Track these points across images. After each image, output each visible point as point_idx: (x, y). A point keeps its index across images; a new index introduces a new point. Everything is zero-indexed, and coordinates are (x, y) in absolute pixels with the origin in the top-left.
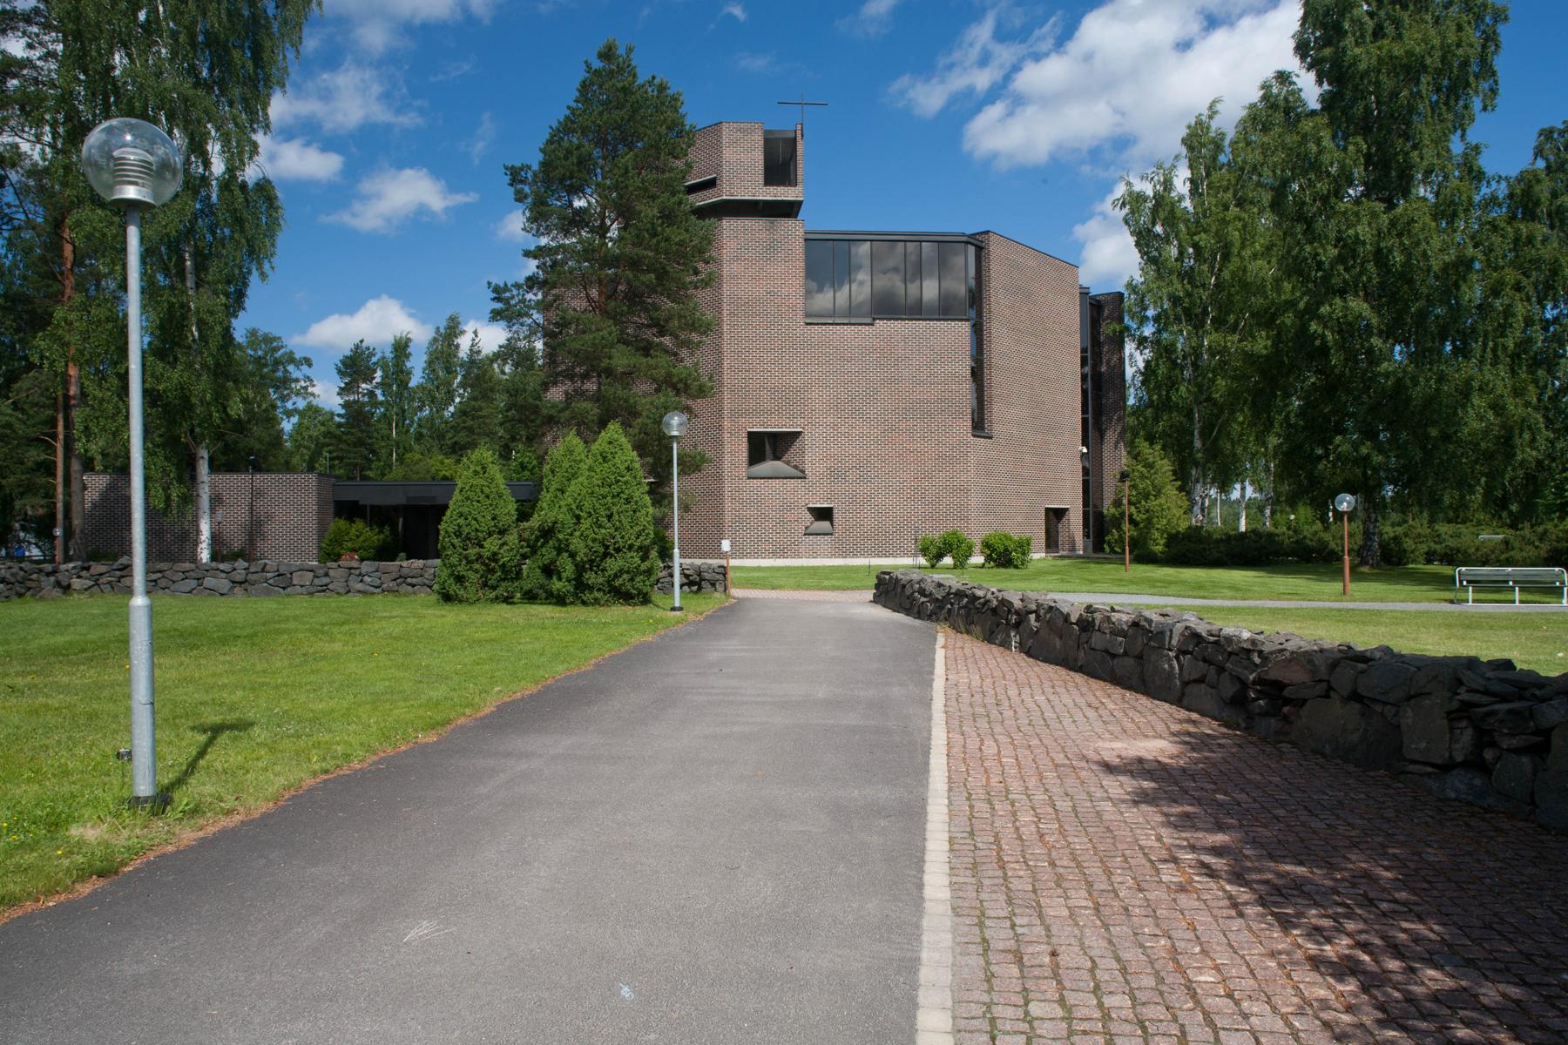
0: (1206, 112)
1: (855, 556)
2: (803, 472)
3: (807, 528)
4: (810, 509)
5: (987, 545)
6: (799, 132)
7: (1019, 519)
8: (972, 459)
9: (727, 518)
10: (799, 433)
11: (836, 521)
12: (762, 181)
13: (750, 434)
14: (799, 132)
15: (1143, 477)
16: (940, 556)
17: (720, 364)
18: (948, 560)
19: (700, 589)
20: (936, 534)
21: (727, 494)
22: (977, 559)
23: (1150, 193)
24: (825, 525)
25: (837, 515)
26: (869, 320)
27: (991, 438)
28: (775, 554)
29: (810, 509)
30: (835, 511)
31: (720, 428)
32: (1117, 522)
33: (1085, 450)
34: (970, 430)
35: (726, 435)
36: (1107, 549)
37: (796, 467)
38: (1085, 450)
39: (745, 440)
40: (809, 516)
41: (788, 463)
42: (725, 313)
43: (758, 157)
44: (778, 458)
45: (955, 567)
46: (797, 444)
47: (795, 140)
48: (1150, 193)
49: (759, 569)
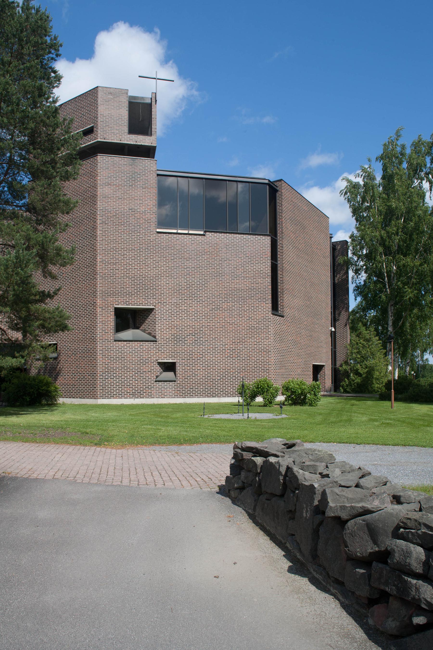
0: (394, 137)
1: (191, 396)
2: (155, 337)
3: (157, 377)
4: (160, 364)
5: (287, 389)
6: (154, 100)
7: (299, 372)
8: (272, 330)
9: (99, 369)
10: (152, 310)
11: (178, 372)
12: (126, 129)
13: (116, 309)
14: (154, 100)
15: (364, 347)
16: (253, 397)
17: (95, 259)
18: (259, 399)
19: (398, 527)
20: (250, 382)
21: (99, 352)
22: (280, 398)
23: (362, 183)
24: (170, 375)
25: (178, 368)
26: (202, 233)
27: (283, 316)
28: (134, 395)
29: (160, 364)
30: (177, 365)
31: (94, 304)
32: (347, 374)
33: (333, 330)
34: (270, 310)
35: (99, 310)
36: (342, 390)
37: (150, 334)
38: (333, 330)
39: (113, 313)
40: (159, 368)
41: (144, 331)
42: (98, 222)
43: (124, 113)
44: (138, 328)
45: (265, 405)
46: (151, 317)
47: (151, 105)
48: (362, 183)
49: (229, 420)
